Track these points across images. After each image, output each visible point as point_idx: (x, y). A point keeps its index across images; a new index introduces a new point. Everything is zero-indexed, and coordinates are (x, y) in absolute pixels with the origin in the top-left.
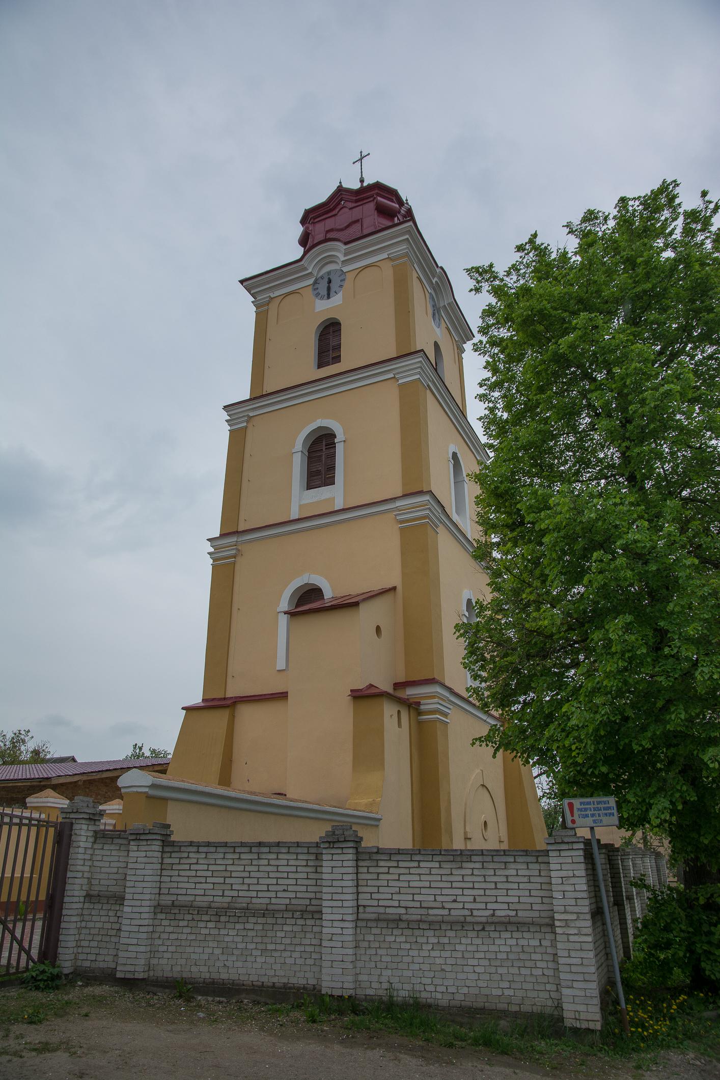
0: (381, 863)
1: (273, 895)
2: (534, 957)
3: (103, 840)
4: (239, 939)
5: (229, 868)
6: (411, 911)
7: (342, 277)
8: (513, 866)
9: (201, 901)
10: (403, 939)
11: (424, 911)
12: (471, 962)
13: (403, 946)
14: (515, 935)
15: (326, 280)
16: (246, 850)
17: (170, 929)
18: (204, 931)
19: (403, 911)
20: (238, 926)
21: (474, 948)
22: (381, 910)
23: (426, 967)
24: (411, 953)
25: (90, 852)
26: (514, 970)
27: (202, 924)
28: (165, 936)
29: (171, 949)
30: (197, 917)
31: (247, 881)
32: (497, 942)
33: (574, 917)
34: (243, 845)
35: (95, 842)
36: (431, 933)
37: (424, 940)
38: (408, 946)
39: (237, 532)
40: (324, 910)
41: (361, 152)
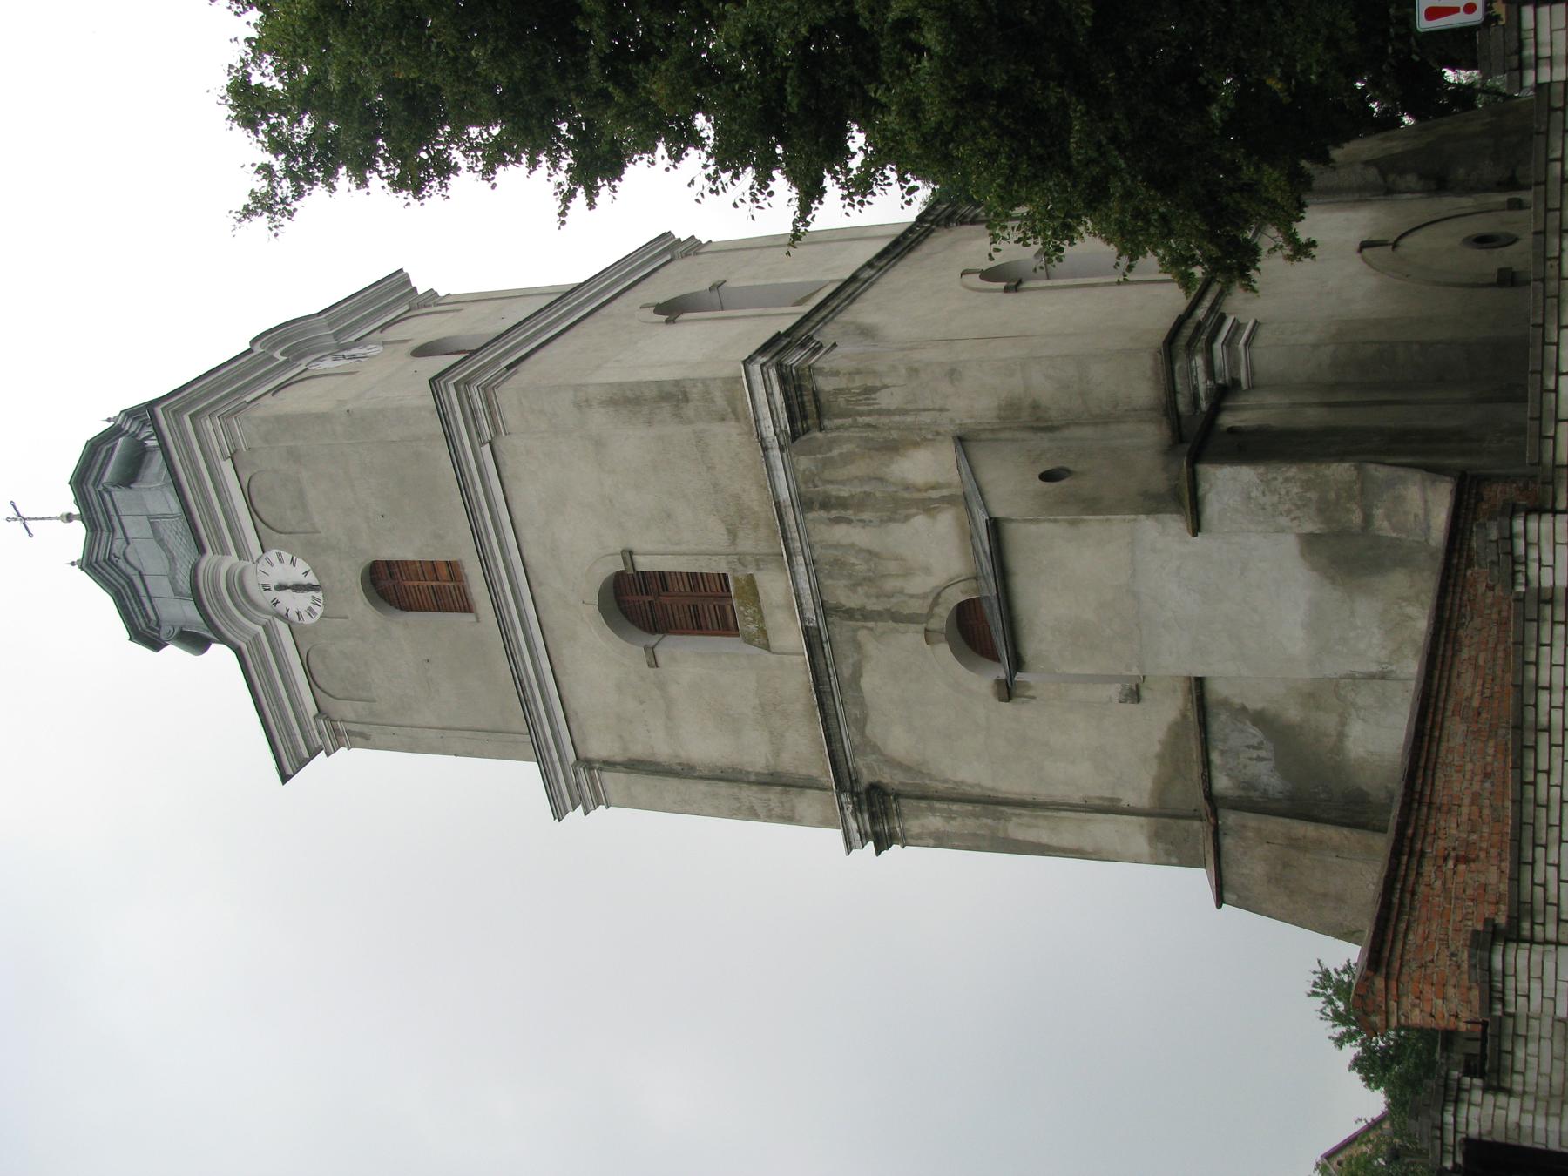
35: (1509, 1092)
41: (8, 519)
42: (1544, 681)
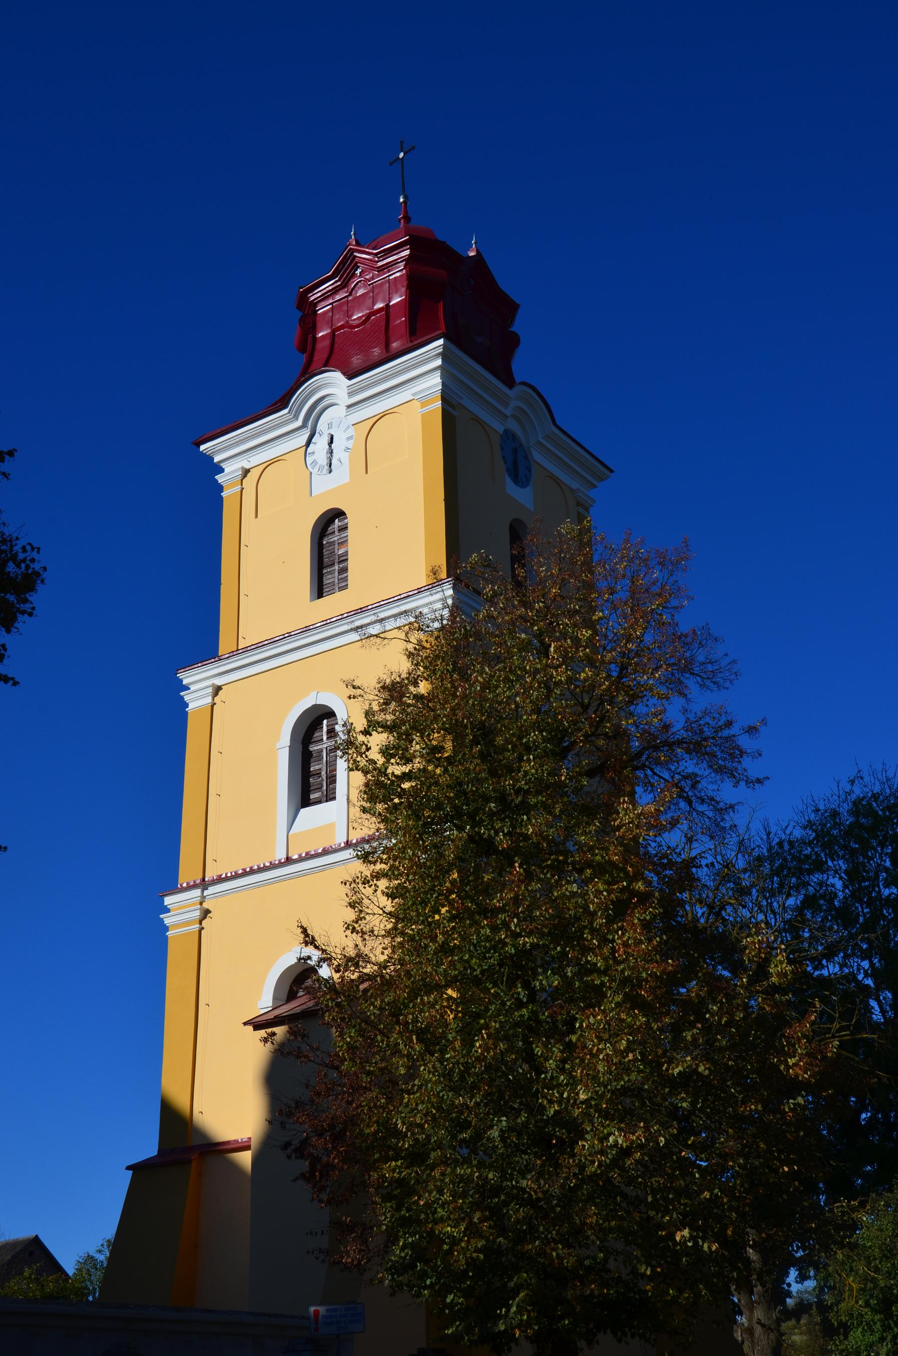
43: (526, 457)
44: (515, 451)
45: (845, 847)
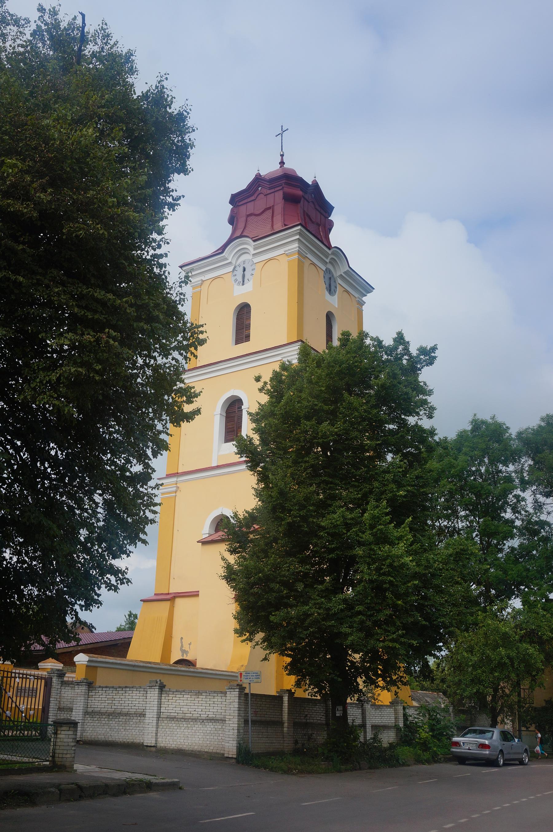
0: (170, 695)
1: (130, 708)
2: (219, 732)
3: (65, 685)
4: (116, 725)
5: (114, 697)
6: (179, 714)
7: (253, 267)
8: (216, 697)
9: (103, 710)
10: (175, 725)
11: (184, 715)
12: (198, 734)
13: (175, 728)
14: (214, 724)
15: (242, 269)
16: (121, 689)
17: (91, 721)
18: (103, 722)
19: (176, 714)
20: (116, 720)
21: (199, 729)
22: (169, 714)
23: (182, 736)
24: (177, 730)
25: (59, 690)
26: (212, 737)
27: (102, 719)
28: (88, 724)
29: (91, 729)
30: (101, 717)
31: (120, 702)
32: (207, 726)
33: (232, 717)
34: (119, 687)
35: (61, 686)
36: (185, 723)
37: (182, 725)
38: (176, 728)
39: (178, 473)
40: (147, 713)
41: (282, 127)
42: (134, 692)
43: (335, 282)
44: (330, 278)
45: (427, 434)
